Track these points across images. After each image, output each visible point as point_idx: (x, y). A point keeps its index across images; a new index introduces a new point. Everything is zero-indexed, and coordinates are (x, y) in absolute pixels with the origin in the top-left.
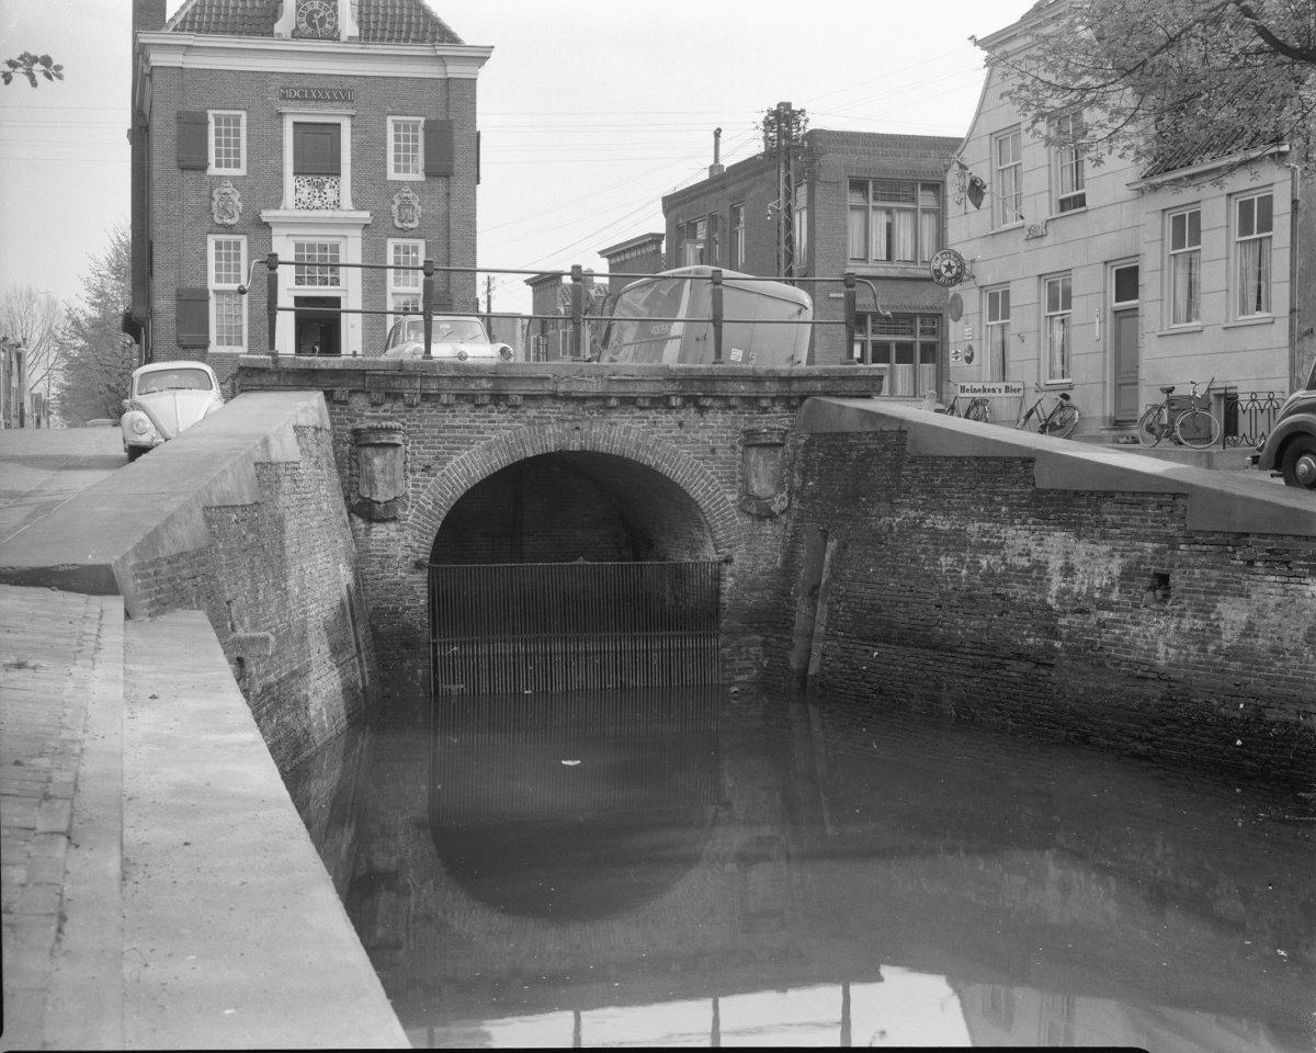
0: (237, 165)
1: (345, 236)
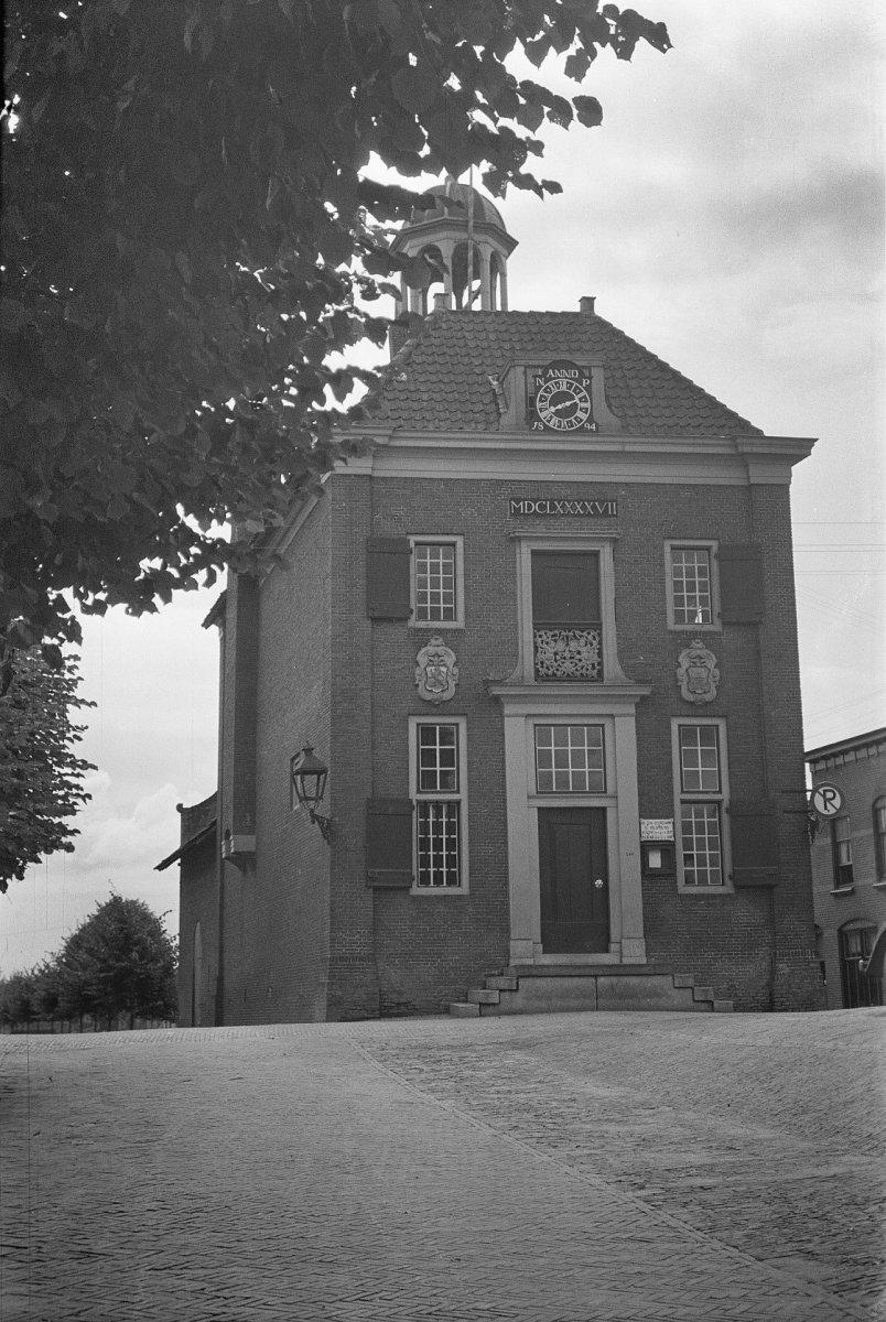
0: (453, 880)
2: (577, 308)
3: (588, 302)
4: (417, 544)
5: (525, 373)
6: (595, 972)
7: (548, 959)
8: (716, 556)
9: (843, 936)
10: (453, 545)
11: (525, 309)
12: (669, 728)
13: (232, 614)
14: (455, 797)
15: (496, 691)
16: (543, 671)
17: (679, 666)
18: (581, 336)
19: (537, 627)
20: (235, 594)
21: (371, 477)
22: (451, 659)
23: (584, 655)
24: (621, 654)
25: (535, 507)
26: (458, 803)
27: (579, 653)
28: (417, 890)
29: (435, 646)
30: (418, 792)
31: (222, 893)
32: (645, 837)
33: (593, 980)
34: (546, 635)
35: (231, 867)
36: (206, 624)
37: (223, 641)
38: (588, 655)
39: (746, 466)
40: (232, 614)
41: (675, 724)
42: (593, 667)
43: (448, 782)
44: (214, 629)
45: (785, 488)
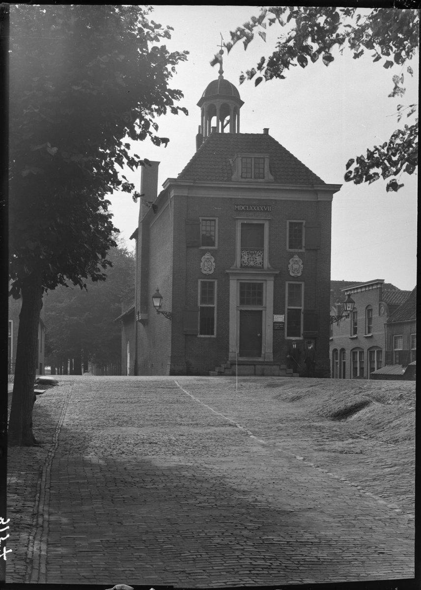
1: (266, 280)
2: (262, 132)
3: (266, 130)
4: (203, 220)
5: (241, 160)
6: (254, 364)
7: (241, 359)
8: (305, 226)
9: (354, 354)
10: (215, 220)
11: (244, 133)
12: (285, 285)
13: (140, 237)
14: (212, 306)
15: (228, 271)
16: (243, 265)
17: (289, 263)
18: (264, 142)
19: (242, 250)
20: (141, 230)
21: (188, 196)
22: (213, 260)
23: (257, 260)
24: (270, 259)
25: (243, 208)
26: (214, 307)
27: (256, 259)
28: (199, 336)
29: (207, 256)
30: (201, 304)
31: (137, 329)
32: (275, 320)
33: (253, 367)
34: (245, 253)
35: (140, 324)
36: (131, 238)
37: (137, 244)
38: (259, 260)
39: (317, 194)
40: (140, 237)
41: (287, 283)
42: (260, 264)
43: (211, 300)
44: (134, 240)
45: (330, 203)
